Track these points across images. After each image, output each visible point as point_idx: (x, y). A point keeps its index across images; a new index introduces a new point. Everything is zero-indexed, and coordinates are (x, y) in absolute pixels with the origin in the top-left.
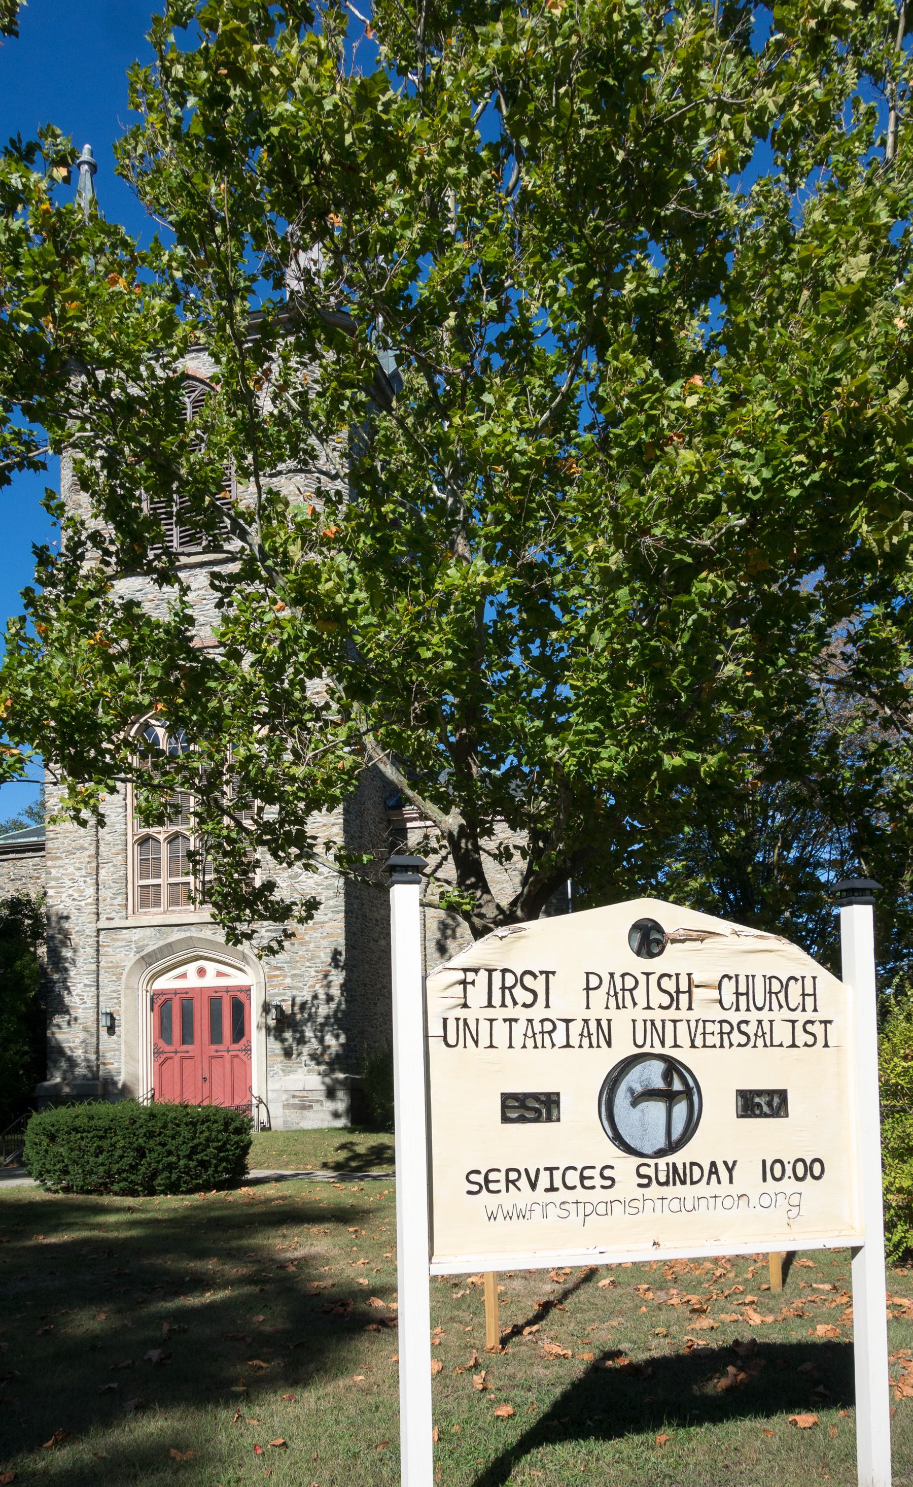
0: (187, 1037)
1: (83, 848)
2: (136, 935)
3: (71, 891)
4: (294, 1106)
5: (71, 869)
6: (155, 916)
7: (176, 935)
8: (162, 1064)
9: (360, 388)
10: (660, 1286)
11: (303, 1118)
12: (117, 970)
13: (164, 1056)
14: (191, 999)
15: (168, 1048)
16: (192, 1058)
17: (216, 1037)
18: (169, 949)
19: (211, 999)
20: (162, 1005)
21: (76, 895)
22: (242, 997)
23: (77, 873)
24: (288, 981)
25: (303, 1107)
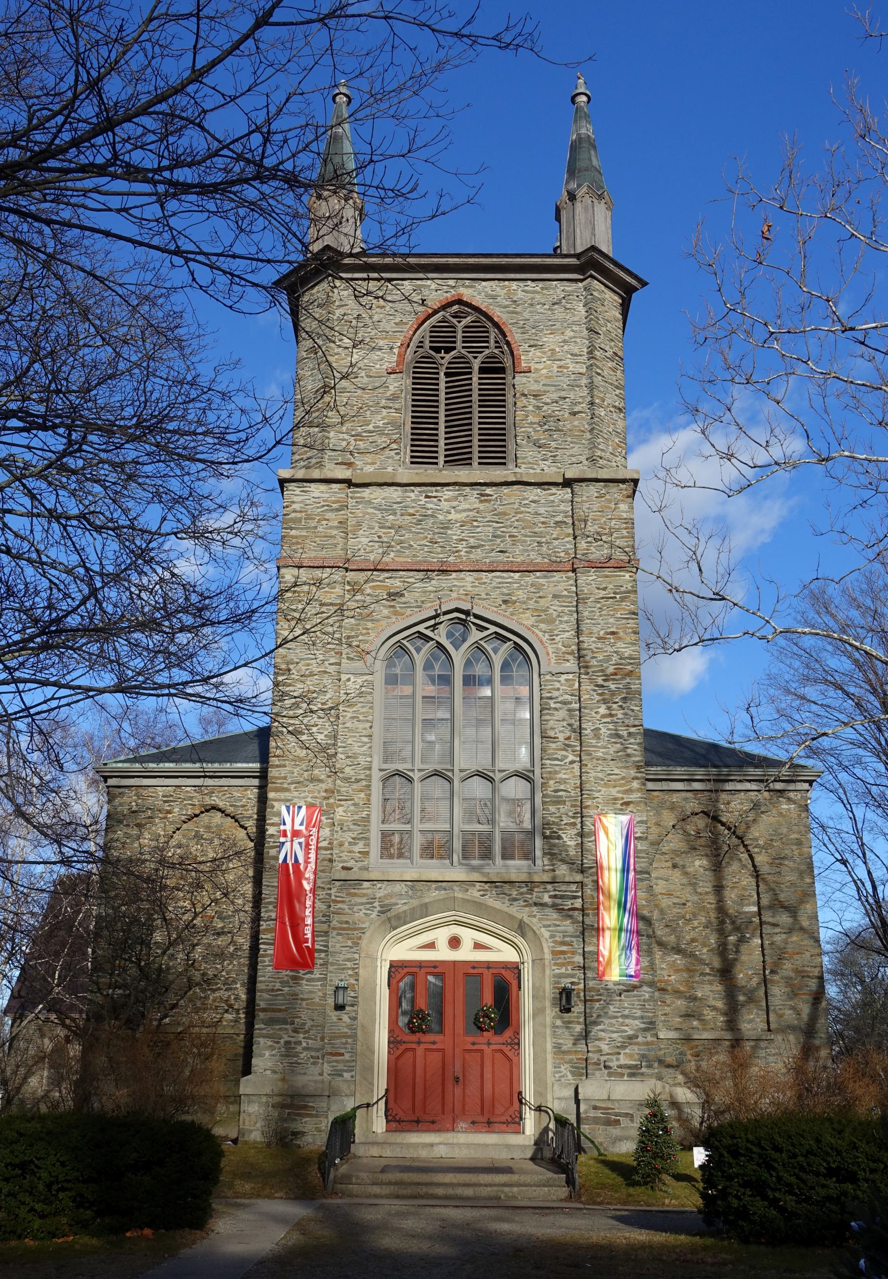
13: (402, 1048)
22: (509, 976)
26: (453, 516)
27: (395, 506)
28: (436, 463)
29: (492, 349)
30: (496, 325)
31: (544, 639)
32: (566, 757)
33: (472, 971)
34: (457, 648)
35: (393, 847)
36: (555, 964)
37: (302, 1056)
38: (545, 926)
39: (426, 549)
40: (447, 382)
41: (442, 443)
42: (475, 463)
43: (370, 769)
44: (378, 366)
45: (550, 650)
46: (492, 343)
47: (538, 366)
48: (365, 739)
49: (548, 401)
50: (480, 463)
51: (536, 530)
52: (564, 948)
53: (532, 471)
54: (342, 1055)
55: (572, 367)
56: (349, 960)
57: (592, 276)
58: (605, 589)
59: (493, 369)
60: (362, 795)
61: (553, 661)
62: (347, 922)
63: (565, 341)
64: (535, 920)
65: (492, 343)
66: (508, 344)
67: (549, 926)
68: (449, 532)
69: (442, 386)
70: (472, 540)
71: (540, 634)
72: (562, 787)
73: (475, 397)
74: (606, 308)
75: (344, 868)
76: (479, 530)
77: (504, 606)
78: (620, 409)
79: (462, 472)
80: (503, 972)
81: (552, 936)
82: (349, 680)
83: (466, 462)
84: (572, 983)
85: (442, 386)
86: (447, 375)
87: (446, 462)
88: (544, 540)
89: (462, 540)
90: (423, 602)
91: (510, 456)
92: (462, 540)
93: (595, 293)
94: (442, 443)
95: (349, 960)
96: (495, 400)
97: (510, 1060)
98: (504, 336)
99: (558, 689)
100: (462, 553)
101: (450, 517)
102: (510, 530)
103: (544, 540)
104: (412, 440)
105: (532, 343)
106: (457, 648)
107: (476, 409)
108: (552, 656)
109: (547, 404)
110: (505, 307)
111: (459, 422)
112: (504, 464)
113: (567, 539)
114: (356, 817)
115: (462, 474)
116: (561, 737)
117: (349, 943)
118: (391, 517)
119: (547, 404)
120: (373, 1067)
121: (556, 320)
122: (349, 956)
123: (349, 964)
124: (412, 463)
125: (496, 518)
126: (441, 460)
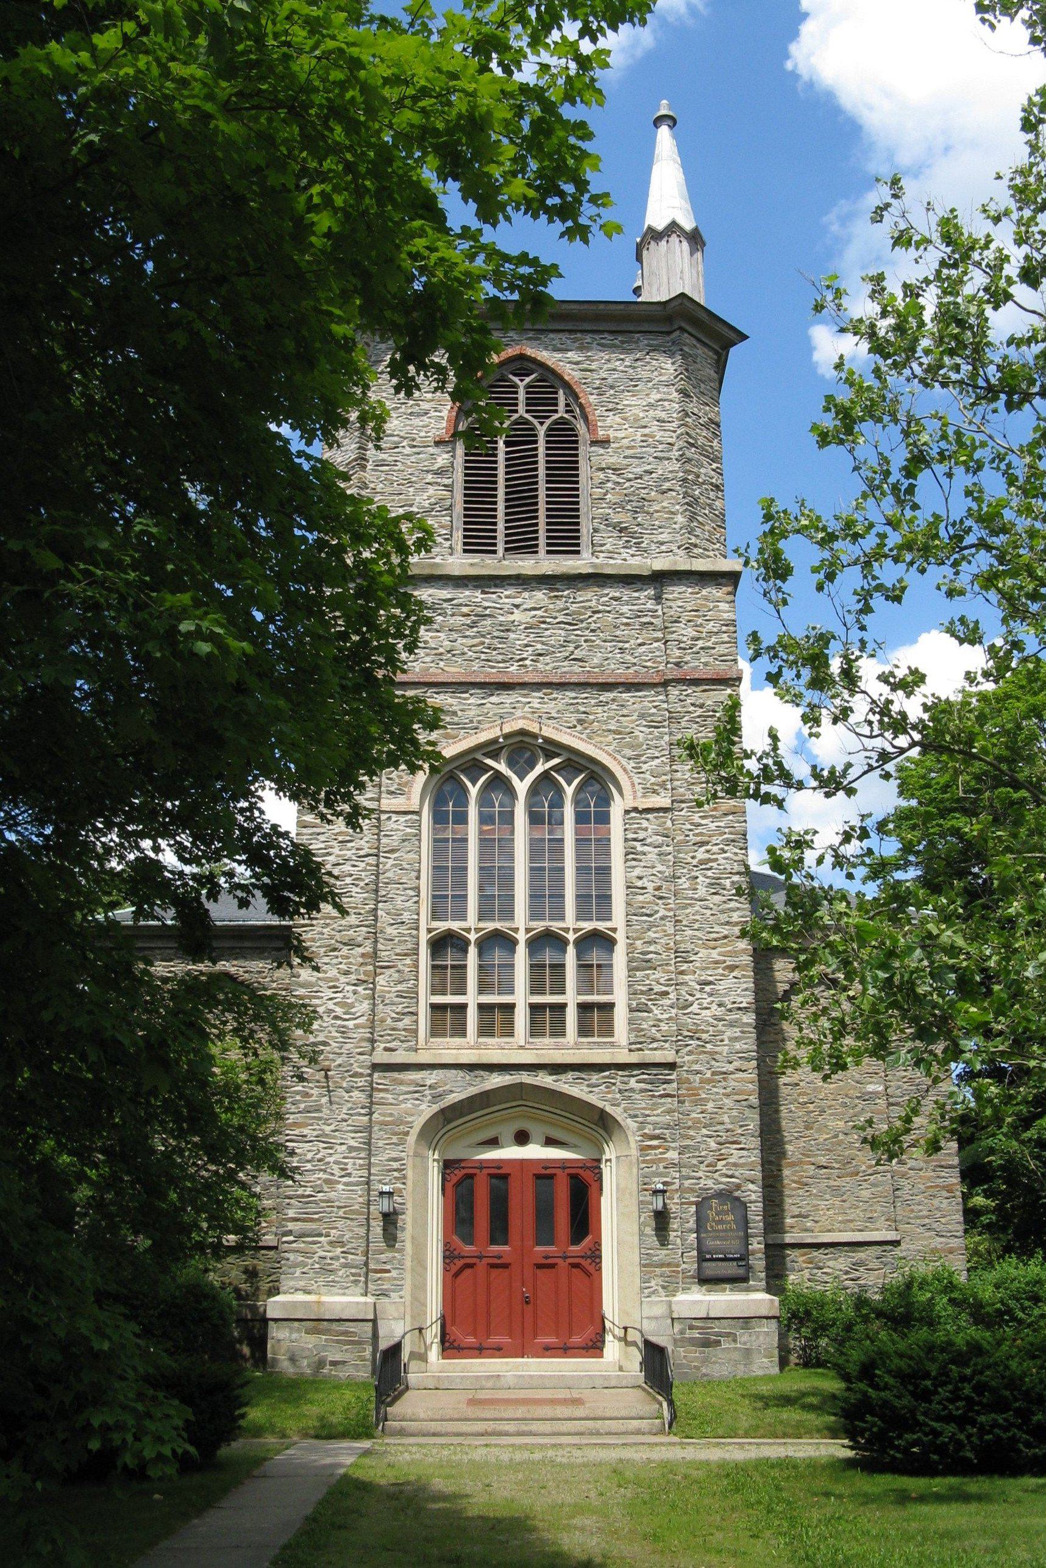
0: (500, 1230)
1: (351, 944)
2: (431, 1077)
3: (330, 1005)
4: (693, 1342)
5: (333, 973)
6: (468, 1047)
7: (496, 1080)
8: (456, 1275)
9: (136, 932)
10: (773, 1466)
11: (705, 1361)
12: (397, 1128)
13: (460, 1263)
14: (505, 1177)
15: (469, 1249)
16: (506, 1266)
17: (544, 1231)
18: (484, 1099)
19: (574, 1177)
20: (460, 1182)
21: (339, 1011)
22: (586, 1175)
23: (343, 979)
24: (673, 1155)
25: (706, 1343)
26: (517, 616)
27: (445, 605)
28: (495, 552)
29: (561, 412)
30: (567, 386)
31: (629, 768)
32: (657, 912)
33: (544, 1172)
34: (569, 784)
35: (448, 1019)
36: (644, 1162)
37: (340, 1273)
38: (631, 1116)
39: (483, 656)
40: (507, 453)
41: (501, 526)
42: (542, 548)
43: (417, 929)
44: (423, 434)
45: (637, 781)
46: (561, 407)
47: (620, 434)
48: (412, 893)
49: (631, 476)
50: (548, 552)
51: (618, 633)
52: (655, 1143)
53: (612, 562)
54: (388, 1271)
55: (659, 435)
56: (395, 1160)
57: (682, 329)
58: (701, 706)
59: (564, 438)
60: (408, 961)
61: (639, 794)
62: (391, 1115)
63: (650, 405)
64: (619, 1110)
65: (561, 407)
66: (581, 406)
67: (636, 1116)
68: (512, 636)
69: (501, 457)
70: (539, 646)
71: (624, 762)
72: (652, 948)
73: (542, 472)
74: (699, 366)
75: (386, 1049)
76: (548, 633)
77: (579, 728)
78: (717, 486)
79: (526, 563)
80: (580, 1171)
81: (640, 1129)
82: (389, 818)
83: (531, 549)
84: (664, 1183)
85: (501, 457)
86: (508, 444)
87: (506, 550)
88: (627, 645)
89: (527, 646)
90: (479, 722)
91: (585, 540)
92: (527, 646)
93: (686, 349)
94: (501, 526)
95: (395, 1160)
96: (565, 471)
97: (588, 1274)
98: (576, 397)
99: (646, 829)
100: (528, 662)
101: (511, 618)
102: (587, 632)
103: (627, 645)
104: (465, 523)
105: (611, 406)
106: (569, 784)
107: (542, 486)
108: (638, 787)
109: (630, 480)
110: (577, 363)
111: (522, 500)
112: (578, 552)
113: (655, 645)
114: (400, 987)
115: (526, 565)
116: (651, 886)
117: (395, 1140)
118: (440, 618)
119: (630, 480)
120: (425, 1285)
121: (639, 379)
122: (394, 1155)
123: (395, 1165)
124: (465, 551)
125: (569, 619)
126: (500, 548)
